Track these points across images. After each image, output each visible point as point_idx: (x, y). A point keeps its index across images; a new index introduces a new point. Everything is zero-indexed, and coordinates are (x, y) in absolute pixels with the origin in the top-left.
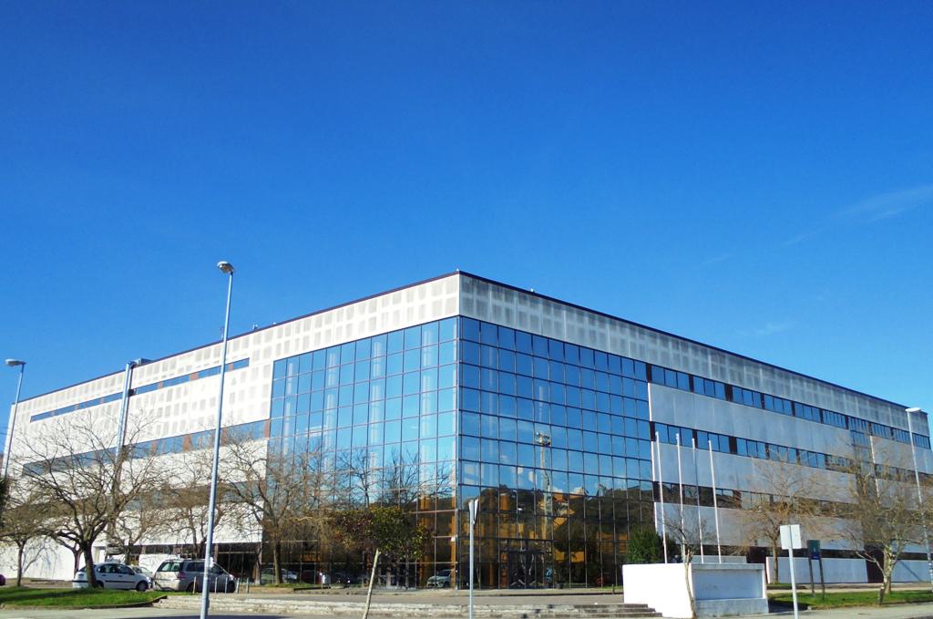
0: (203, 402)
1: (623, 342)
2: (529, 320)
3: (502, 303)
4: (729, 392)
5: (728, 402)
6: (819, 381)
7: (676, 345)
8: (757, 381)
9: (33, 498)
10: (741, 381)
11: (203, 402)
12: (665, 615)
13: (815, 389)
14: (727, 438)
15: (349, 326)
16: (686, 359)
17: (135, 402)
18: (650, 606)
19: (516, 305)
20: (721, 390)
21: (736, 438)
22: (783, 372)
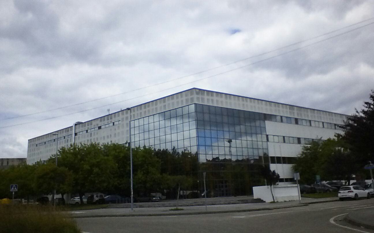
0: (104, 137)
1: (255, 107)
2: (201, 100)
3: (210, 98)
4: (297, 121)
5: (296, 125)
6: (322, 111)
7: (217, 96)
8: (308, 116)
9: (301, 156)
10: (294, 115)
11: (104, 137)
12: (267, 201)
13: (320, 114)
14: (282, 137)
15: (156, 108)
16: (279, 110)
17: (78, 138)
18: (262, 199)
19: (215, 98)
20: (293, 121)
21: (300, 138)
22: (276, 104)
